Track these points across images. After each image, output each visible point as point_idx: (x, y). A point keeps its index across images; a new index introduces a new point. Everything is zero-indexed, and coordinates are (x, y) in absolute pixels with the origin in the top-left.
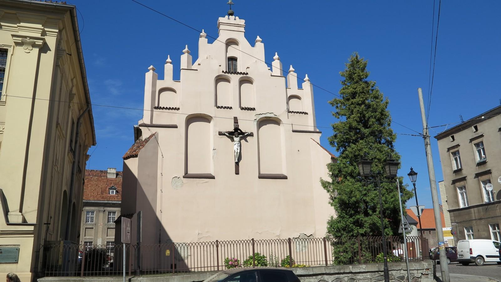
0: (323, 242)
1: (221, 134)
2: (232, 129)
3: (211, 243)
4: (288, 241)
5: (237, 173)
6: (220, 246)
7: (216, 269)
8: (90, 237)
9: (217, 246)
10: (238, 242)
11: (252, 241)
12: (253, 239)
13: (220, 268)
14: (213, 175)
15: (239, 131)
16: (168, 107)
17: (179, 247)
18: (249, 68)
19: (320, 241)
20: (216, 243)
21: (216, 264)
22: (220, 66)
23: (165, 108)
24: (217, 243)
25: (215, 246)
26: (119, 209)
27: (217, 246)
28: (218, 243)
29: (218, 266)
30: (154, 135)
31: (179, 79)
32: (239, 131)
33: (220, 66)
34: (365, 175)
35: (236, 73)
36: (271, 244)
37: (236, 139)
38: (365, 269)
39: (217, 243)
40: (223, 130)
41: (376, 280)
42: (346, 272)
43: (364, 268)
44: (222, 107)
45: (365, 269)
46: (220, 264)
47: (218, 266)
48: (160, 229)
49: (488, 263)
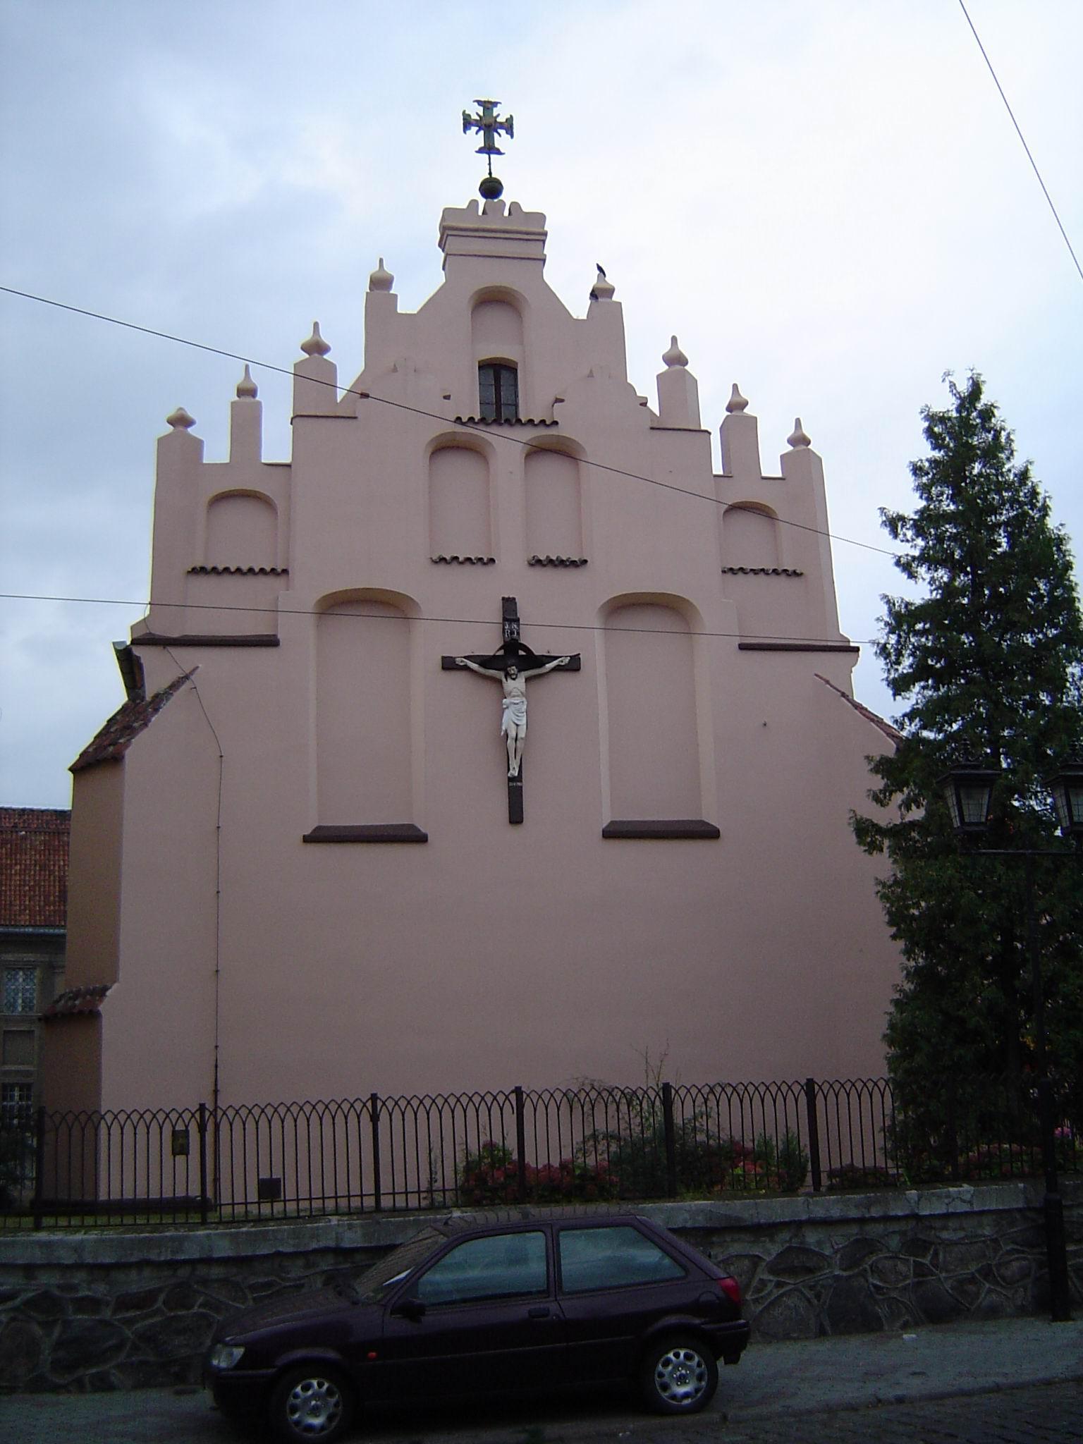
0: (803, 1099)
1: (449, 664)
2: (491, 645)
3: (495, 1098)
4: (805, 1088)
5: (516, 817)
6: (384, 1116)
7: (369, 1202)
8: (21, 1067)
9: (375, 1118)
10: (768, 1088)
11: (513, 1097)
12: (518, 1091)
13: (386, 1202)
14: (423, 830)
15: (521, 653)
16: (245, 568)
17: (76, 1123)
18: (562, 401)
19: (790, 1097)
20: (369, 1104)
21: (369, 1187)
22: (447, 397)
23: (233, 569)
24: (374, 1106)
25: (365, 1117)
26: (516, 774)
27: (375, 1118)
28: (379, 1104)
29: (377, 1194)
30: (187, 677)
31: (118, 652)
32: (521, 653)
33: (447, 397)
34: (967, 828)
35: (515, 421)
36: (683, 1103)
37: (516, 685)
38: (969, 1202)
39: (374, 1106)
40: (458, 652)
41: (1017, 1244)
42: (892, 1213)
43: (968, 1197)
44: (456, 558)
45: (969, 1202)
46: (385, 1186)
47: (377, 1194)
48: (214, 1044)
49: (106, 1137)
